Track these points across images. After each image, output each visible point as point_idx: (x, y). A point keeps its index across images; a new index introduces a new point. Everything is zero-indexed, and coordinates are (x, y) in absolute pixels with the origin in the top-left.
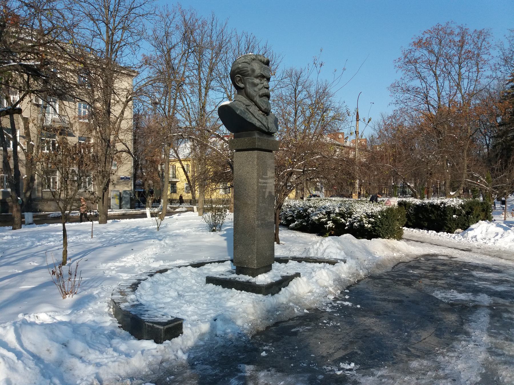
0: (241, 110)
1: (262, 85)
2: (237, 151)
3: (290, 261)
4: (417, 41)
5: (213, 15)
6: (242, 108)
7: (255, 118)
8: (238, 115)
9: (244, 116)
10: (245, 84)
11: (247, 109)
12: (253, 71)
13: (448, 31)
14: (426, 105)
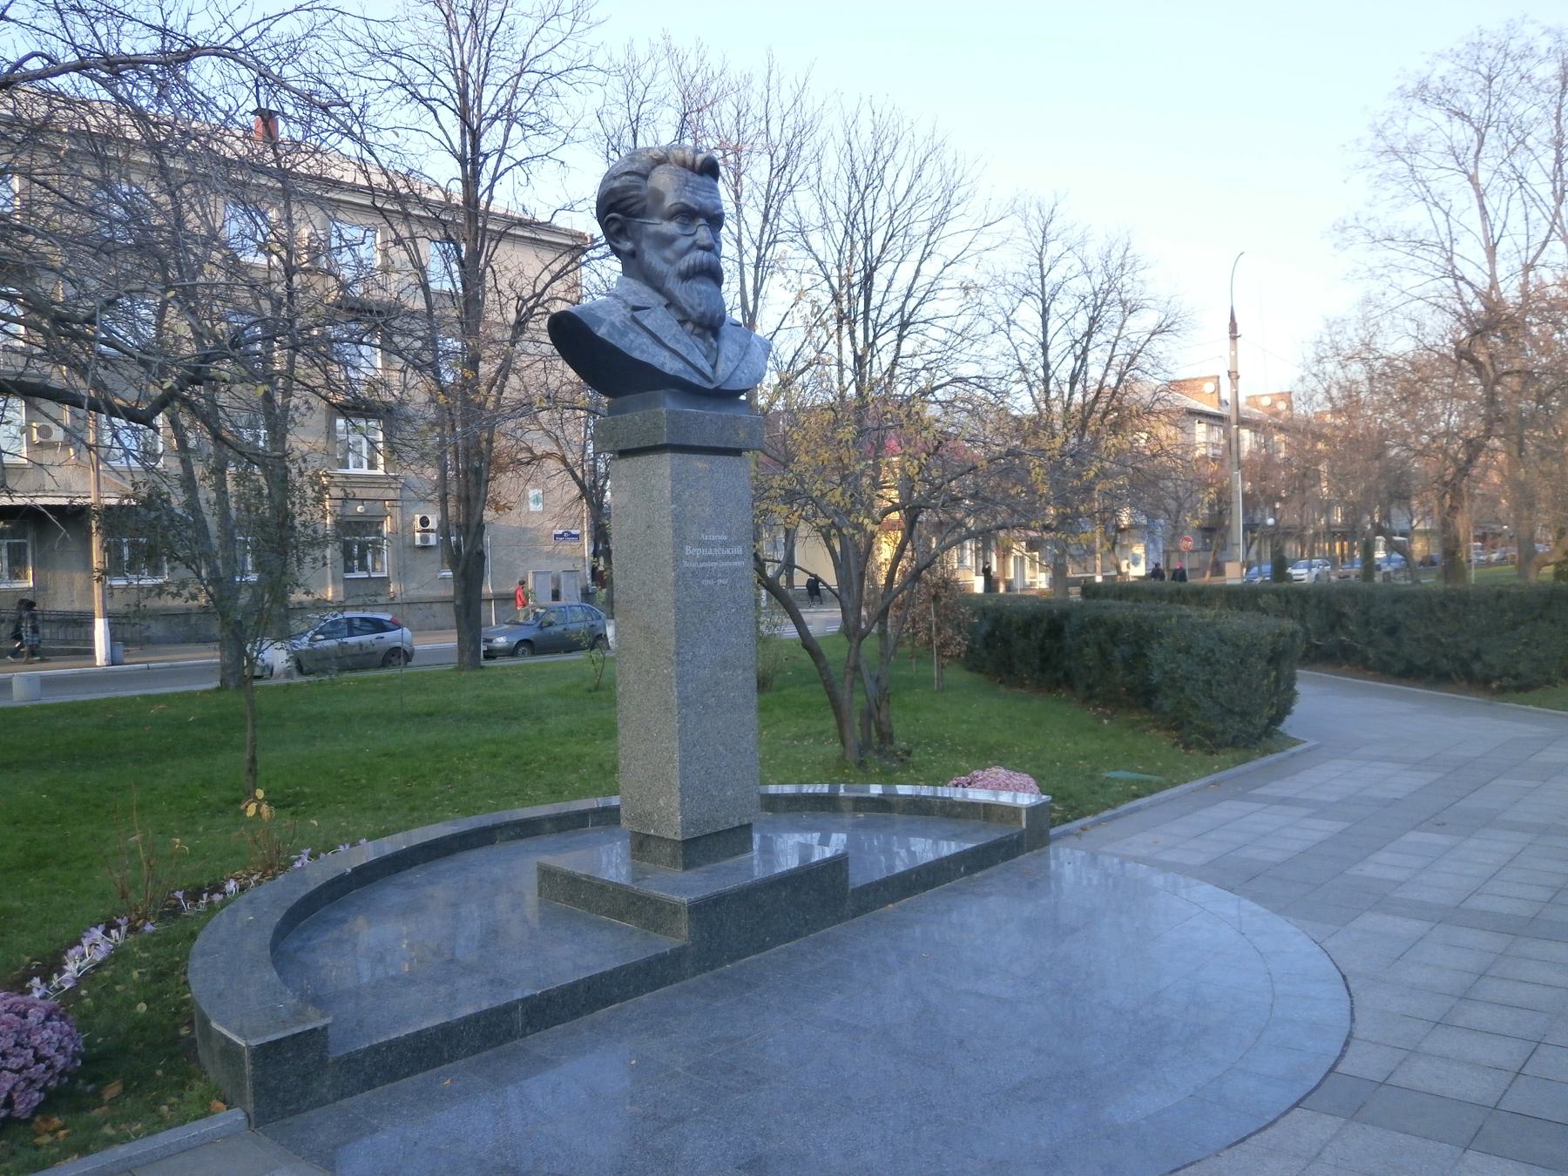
0: (613, 325)
1: (690, 240)
2: (624, 454)
3: (1319, 700)
4: (1411, 86)
5: (770, 56)
6: (619, 315)
7: (663, 347)
8: (601, 343)
9: (621, 343)
10: (637, 243)
11: (635, 320)
12: (659, 197)
13: (1515, 47)
14: (1450, 282)
